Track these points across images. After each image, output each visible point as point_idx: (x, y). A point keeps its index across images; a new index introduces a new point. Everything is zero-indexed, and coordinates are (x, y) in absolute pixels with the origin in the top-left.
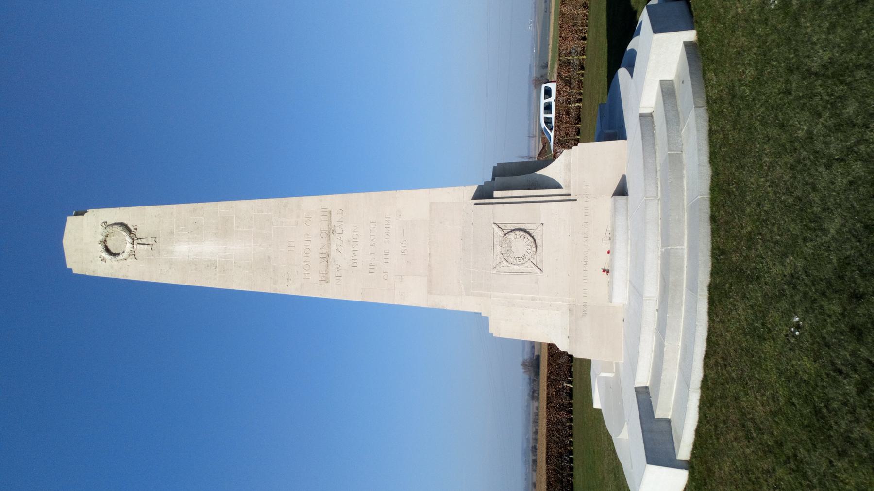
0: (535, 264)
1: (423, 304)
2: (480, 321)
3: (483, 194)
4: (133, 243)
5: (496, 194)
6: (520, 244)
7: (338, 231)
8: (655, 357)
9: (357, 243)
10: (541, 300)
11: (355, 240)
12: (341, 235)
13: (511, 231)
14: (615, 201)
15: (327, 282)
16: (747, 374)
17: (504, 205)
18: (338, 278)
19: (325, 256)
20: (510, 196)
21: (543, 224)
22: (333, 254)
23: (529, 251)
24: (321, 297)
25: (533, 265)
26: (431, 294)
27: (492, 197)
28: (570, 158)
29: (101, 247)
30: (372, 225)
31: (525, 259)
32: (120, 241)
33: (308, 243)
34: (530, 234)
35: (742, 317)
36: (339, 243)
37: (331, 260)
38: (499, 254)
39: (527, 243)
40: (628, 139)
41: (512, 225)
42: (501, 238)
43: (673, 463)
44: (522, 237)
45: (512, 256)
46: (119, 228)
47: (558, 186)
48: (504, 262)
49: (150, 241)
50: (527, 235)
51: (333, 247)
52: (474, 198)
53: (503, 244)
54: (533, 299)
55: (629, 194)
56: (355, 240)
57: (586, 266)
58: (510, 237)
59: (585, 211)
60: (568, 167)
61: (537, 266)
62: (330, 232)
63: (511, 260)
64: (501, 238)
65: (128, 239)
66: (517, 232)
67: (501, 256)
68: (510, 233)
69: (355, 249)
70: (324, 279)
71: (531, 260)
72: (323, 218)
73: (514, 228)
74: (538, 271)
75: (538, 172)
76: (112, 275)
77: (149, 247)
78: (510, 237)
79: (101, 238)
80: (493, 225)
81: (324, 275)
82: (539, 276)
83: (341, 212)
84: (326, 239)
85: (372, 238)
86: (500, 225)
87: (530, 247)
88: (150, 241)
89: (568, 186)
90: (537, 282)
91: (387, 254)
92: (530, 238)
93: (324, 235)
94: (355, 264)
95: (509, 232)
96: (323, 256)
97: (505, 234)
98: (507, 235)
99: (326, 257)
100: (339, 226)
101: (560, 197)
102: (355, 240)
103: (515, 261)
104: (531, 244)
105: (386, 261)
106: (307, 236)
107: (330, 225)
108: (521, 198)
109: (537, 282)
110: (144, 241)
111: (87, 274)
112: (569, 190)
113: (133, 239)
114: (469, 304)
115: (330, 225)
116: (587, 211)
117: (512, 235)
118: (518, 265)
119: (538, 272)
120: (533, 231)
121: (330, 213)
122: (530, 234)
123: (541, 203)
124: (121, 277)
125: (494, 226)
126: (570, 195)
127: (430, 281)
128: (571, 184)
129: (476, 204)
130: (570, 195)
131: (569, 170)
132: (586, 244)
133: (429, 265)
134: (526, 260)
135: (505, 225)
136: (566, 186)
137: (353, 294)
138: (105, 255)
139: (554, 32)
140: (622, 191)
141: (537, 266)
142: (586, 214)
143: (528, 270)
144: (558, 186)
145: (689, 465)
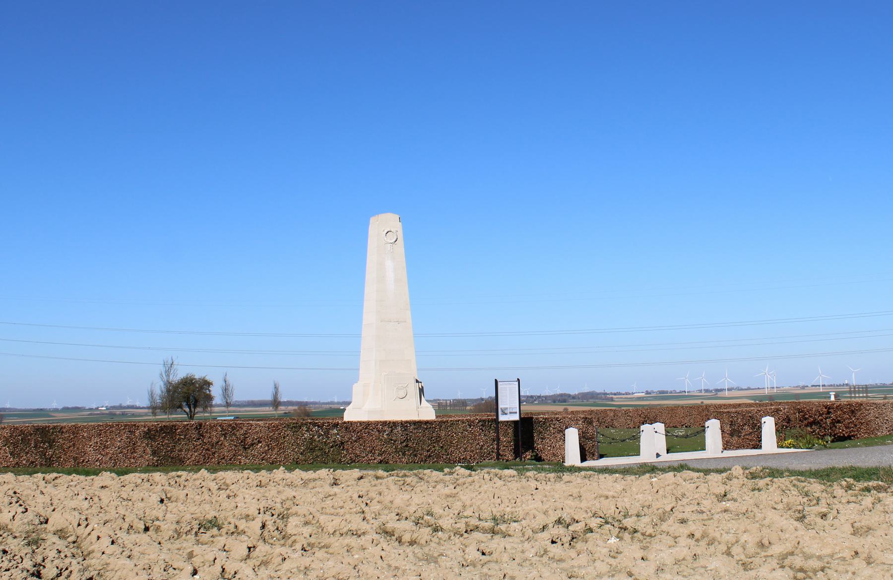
6: (402, 394)
29: (389, 230)
46: (395, 239)
62: (399, 322)
79: (392, 230)
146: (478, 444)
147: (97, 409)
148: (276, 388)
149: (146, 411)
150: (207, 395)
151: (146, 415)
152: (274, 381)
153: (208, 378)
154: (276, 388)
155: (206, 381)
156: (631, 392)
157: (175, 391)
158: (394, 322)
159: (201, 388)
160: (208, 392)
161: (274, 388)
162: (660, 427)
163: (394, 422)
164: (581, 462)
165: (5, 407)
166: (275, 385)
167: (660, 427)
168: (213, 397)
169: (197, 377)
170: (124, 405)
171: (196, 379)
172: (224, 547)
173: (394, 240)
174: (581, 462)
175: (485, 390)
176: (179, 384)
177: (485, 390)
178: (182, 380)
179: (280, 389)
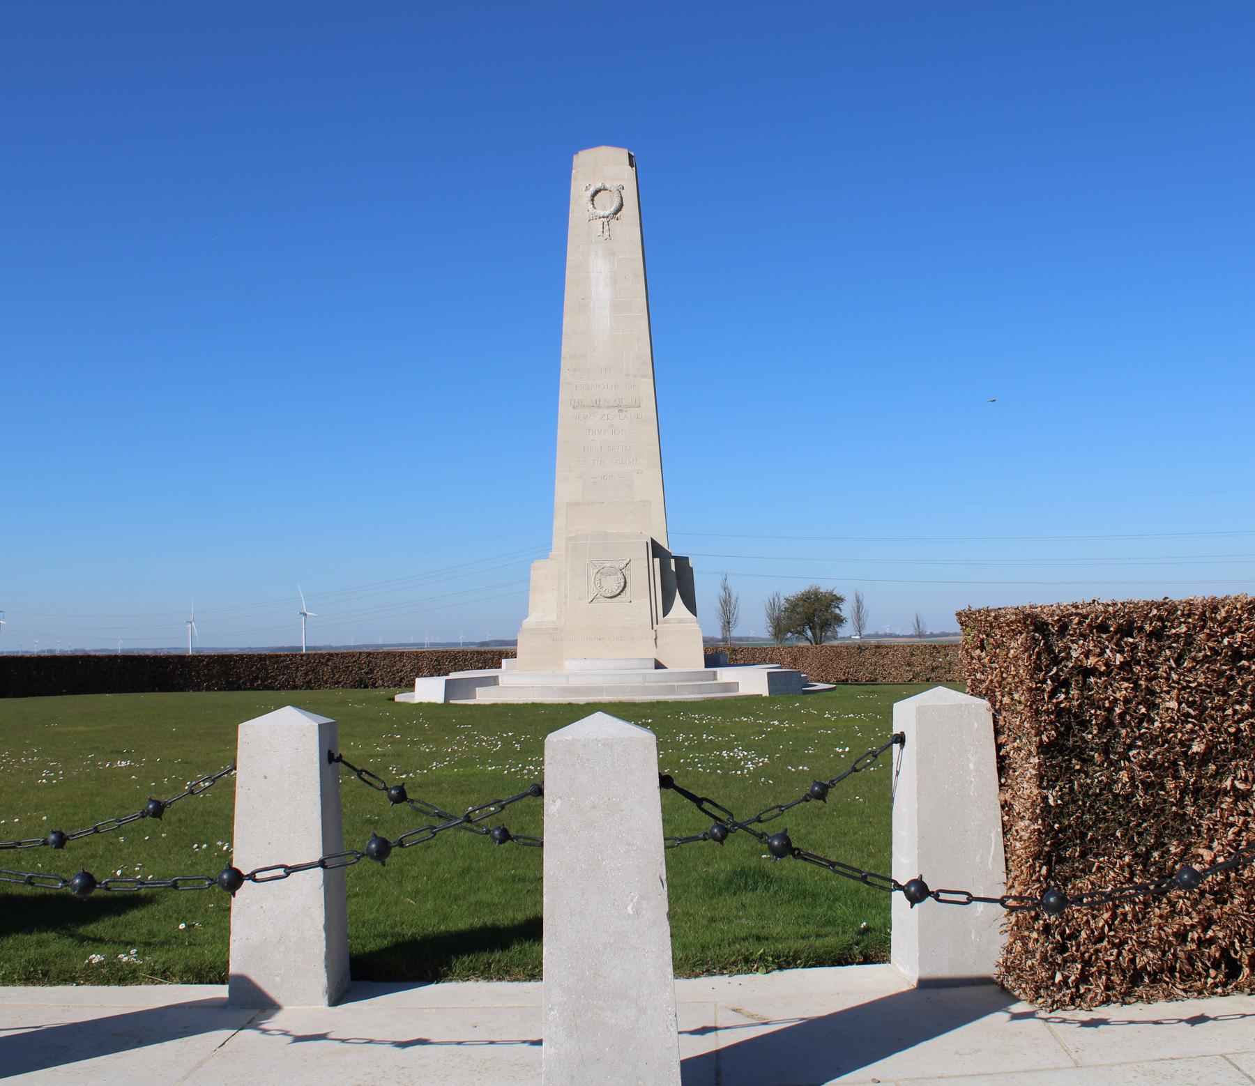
1: (557, 499)
2: (544, 550)
3: (657, 550)
4: (603, 217)
5: (657, 561)
6: (613, 584)
7: (622, 415)
8: (505, 641)
9: (611, 434)
10: (566, 603)
16: (1227, 713)
19: (598, 404)
27: (654, 557)
29: (599, 185)
32: (607, 204)
34: (622, 591)
35: (152, 668)
43: (447, 697)
46: (616, 204)
47: (665, 614)
48: (597, 570)
49: (606, 234)
50: (621, 589)
52: (653, 541)
54: (566, 596)
60: (681, 621)
62: (620, 408)
63: (599, 575)
65: (607, 213)
66: (623, 580)
67: (602, 567)
74: (590, 600)
75: (677, 592)
76: (547, 815)
77: (600, 233)
79: (608, 186)
88: (606, 234)
89: (665, 622)
90: (580, 599)
92: (619, 591)
99: (596, 405)
100: (626, 415)
107: (627, 407)
110: (606, 228)
111: (574, 171)
113: (608, 217)
114: (558, 542)
115: (627, 407)
117: (620, 576)
121: (639, 407)
122: (622, 591)
124: (571, 206)
125: (628, 560)
126: (657, 624)
129: (647, 543)
130: (657, 624)
131: (679, 623)
137: (564, 434)
138: (592, 190)
140: (658, 665)
144: (665, 614)
145: (446, 704)
147: (850, 637)
152: (856, 591)
153: (837, 593)
155: (835, 595)
156: (594, 202)
158: (608, 407)
159: (829, 606)
160: (837, 611)
163: (369, 654)
164: (339, 996)
165: (748, 636)
166: (856, 594)
169: (822, 590)
170: (881, 632)
173: (612, 209)
174: (339, 996)
179: (866, 604)
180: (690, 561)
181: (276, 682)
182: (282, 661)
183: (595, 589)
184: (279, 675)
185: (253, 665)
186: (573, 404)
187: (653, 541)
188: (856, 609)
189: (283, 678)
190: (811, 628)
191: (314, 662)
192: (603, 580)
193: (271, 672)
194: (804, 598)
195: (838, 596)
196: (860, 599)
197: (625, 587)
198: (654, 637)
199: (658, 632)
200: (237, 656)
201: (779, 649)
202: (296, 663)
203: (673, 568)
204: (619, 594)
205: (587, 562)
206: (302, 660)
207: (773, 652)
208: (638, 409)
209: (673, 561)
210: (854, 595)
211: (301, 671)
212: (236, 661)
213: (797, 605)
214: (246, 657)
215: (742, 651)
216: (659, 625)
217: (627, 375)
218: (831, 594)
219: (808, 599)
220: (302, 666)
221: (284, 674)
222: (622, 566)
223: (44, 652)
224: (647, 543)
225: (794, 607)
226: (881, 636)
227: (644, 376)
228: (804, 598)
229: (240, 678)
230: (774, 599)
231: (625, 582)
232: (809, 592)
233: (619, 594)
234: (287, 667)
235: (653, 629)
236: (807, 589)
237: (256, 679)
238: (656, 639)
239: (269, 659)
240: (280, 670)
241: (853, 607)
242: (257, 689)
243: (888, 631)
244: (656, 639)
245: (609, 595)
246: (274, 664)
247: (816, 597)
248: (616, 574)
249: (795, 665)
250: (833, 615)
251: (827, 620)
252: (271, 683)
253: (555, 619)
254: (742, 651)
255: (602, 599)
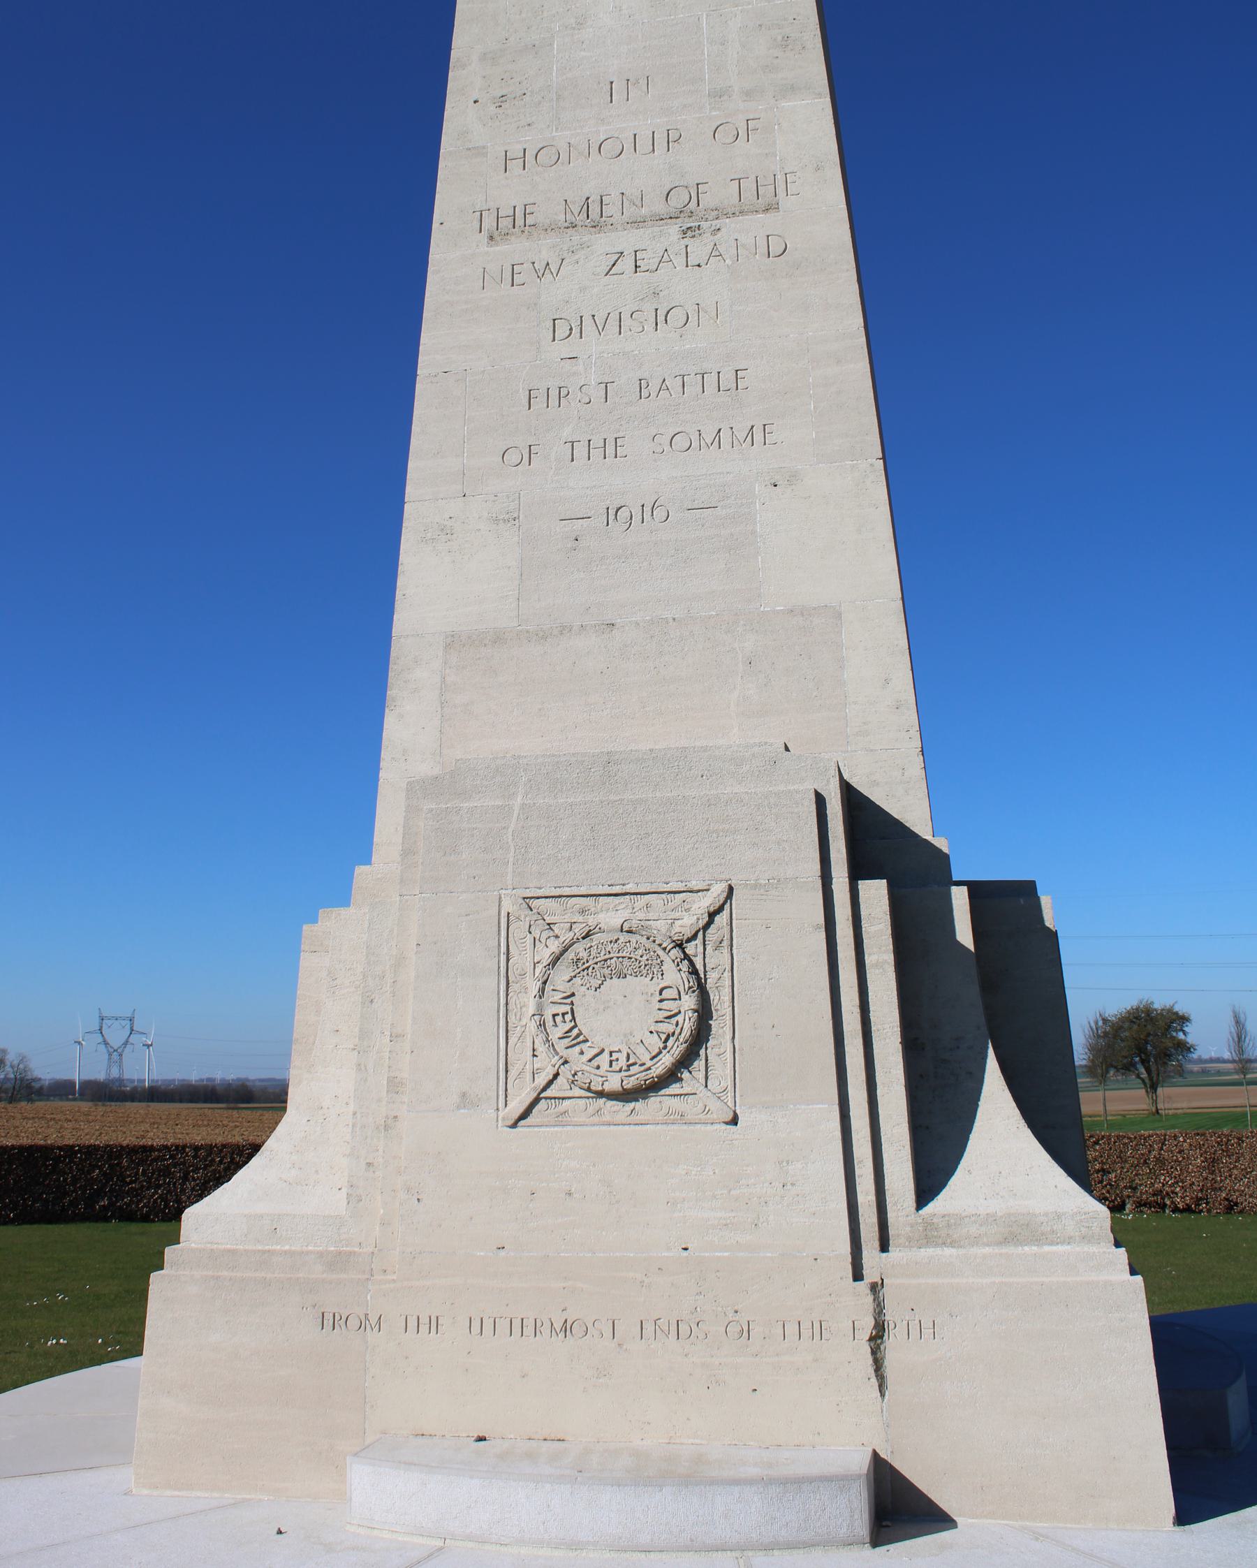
0: (548, 1093)
1: (404, 620)
5: (875, 893)
7: (699, 249)
9: (649, 327)
11: (661, 318)
12: (679, 261)
13: (694, 971)
14: (839, 1480)
15: (491, 238)
17: (823, 935)
18: (508, 275)
20: (869, 960)
21: (734, 1121)
22: (604, 244)
23: (605, 1057)
24: (435, 225)
25: (542, 1080)
26: (448, 646)
27: (858, 871)
28: (1069, 1240)
30: (727, 379)
31: (566, 1042)
33: (644, 143)
34: (685, 1061)
36: (648, 261)
37: (576, 237)
38: (592, 921)
39: (640, 1050)
40: (1177, 1529)
41: (727, 975)
42: (661, 926)
44: (668, 1027)
45: (578, 981)
48: (555, 946)
50: (676, 1049)
51: (627, 240)
52: (848, 791)
53: (634, 938)
55: (881, 1550)
56: (661, 319)
57: (546, 1329)
58: (669, 966)
59: (806, 1325)
61: (537, 1100)
64: (661, 926)
67: (579, 930)
68: (685, 966)
69: (626, 321)
70: (505, 223)
71: (566, 1072)
72: (749, 185)
73: (710, 985)
74: (517, 1105)
75: (992, 1065)
78: (669, 966)
80: (724, 886)
81: (520, 222)
82: (492, 1112)
83: (776, 248)
84: (660, 208)
85: (674, 384)
86: (721, 919)
87: (623, 1063)
89: (929, 1236)
90: (465, 1100)
91: (610, 450)
92: (667, 1060)
93: (678, 200)
94: (562, 331)
95: (692, 963)
96: (595, 209)
97: (680, 945)
98: (676, 953)
101: (872, 1197)
102: (661, 318)
103: (557, 997)
104: (634, 1069)
105: (581, 450)
106: (673, 135)
107: (721, 213)
108: (857, 1011)
109: (465, 1100)
112: (909, 1239)
115: (721, 213)
116: (806, 1333)
117: (675, 976)
118: (539, 1013)
119: (511, 1105)
120: (701, 1075)
122: (685, 1061)
123: (836, 1108)
125: (719, 890)
126: (884, 1247)
127: (499, 639)
128: (938, 1251)
129: (820, 801)
130: (884, 1247)
131: (1010, 1238)
132: (649, 1328)
133: (565, 629)
134: (561, 1046)
135: (726, 943)
136: (929, 1225)
139: (1217, 1112)
141: (537, 1100)
142: (792, 1329)
143: (521, 1056)
146: (203, 1120)
148: (1238, 1022)
149: (1230, 1066)
150: (1174, 1037)
151: (1228, 1073)
152: (1234, 1006)
153: (1180, 1008)
154: (1238, 1022)
155: (1176, 1013)
157: (1115, 1036)
158: (637, 223)
159: (1168, 1027)
160: (1181, 1036)
161: (1233, 1023)
162: (883, 883)
166: (1234, 1012)
167: (883, 883)
168: (1192, 1046)
169: (1156, 1006)
171: (1156, 1010)
172: (657, 1320)
175: (1214, 1049)
176: (1123, 1022)
177: (1214, 1049)
178: (673, 1064)
180: (1046, 901)
181: (141, 1201)
182: (156, 1159)
183: (541, 1048)
184: (148, 1189)
185: (93, 1167)
186: (489, 222)
187: (853, 800)
188: (1235, 1035)
189: (156, 1192)
190: (1143, 1062)
191: (221, 1162)
192: (586, 1002)
193: (131, 1182)
194: (1131, 1017)
195: (1181, 1013)
196: (1242, 1019)
197: (701, 1035)
198: (867, 1325)
199: (887, 1293)
200: (60, 1148)
201: (1175, 1137)
202: (184, 1164)
203: (964, 934)
204: (671, 1076)
205: (507, 906)
206: (195, 1157)
207: (1163, 1144)
208: (771, 216)
209: (960, 898)
210: (1231, 1013)
211: (194, 1179)
212: (57, 1160)
213: (1121, 1027)
214: (79, 1151)
215: (1096, 1143)
216: (894, 1253)
217: (719, 94)
218: (1170, 1011)
219: (1136, 1018)
220: (196, 1170)
221: (158, 1187)
222: (687, 922)
223: (202, 1080)
224: (820, 801)
225: (1116, 1031)
226: (1206, 1061)
227: (790, 90)
228: (1131, 1017)
229: (66, 1194)
230: (1096, 1023)
231: (704, 1012)
232: (1137, 1009)
233: (671, 1076)
234: (166, 1172)
235: (858, 1276)
236: (1135, 1003)
237: (99, 1194)
238: (878, 1336)
239: (128, 1154)
240: (150, 1178)
241: (1231, 1033)
242: (102, 1217)
243: (1213, 1055)
244: (878, 1336)
245: (613, 1084)
246: (138, 1164)
247: (1148, 1015)
248: (651, 968)
249: (1213, 1173)
250: (1176, 1042)
251: (1166, 1048)
252: (128, 1205)
253: (337, 1203)
254: (1096, 1143)
255: (579, 1107)
